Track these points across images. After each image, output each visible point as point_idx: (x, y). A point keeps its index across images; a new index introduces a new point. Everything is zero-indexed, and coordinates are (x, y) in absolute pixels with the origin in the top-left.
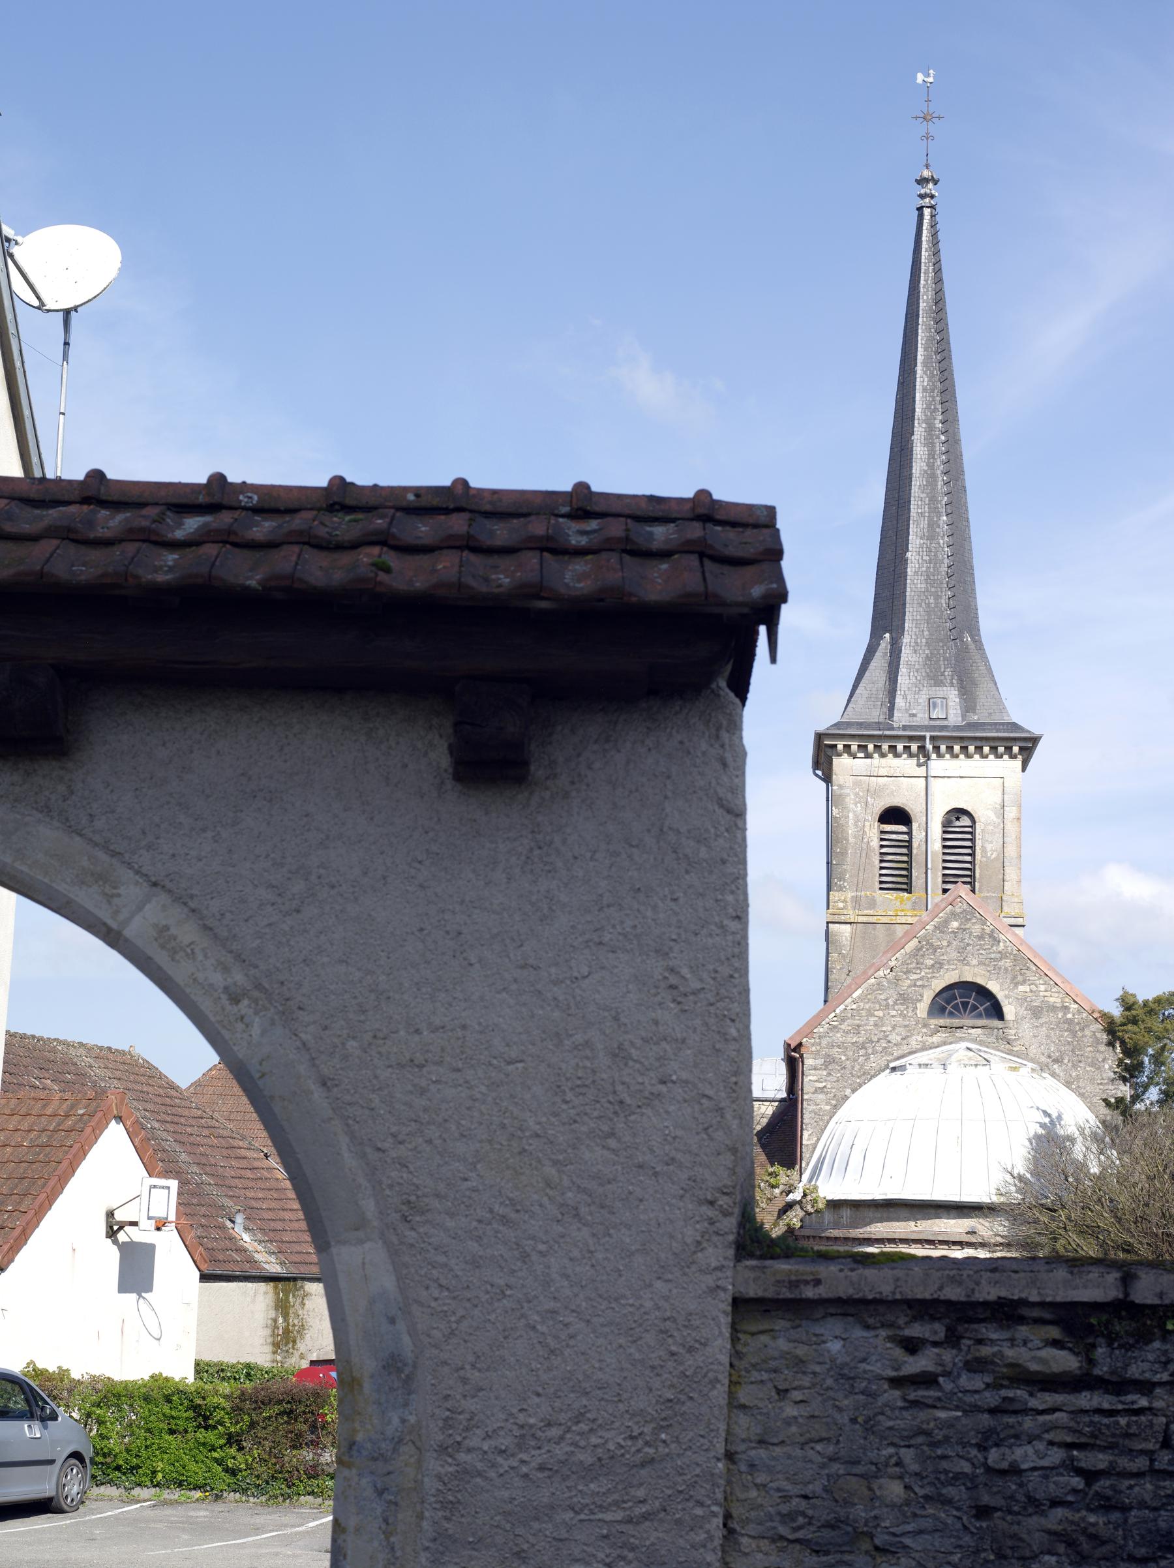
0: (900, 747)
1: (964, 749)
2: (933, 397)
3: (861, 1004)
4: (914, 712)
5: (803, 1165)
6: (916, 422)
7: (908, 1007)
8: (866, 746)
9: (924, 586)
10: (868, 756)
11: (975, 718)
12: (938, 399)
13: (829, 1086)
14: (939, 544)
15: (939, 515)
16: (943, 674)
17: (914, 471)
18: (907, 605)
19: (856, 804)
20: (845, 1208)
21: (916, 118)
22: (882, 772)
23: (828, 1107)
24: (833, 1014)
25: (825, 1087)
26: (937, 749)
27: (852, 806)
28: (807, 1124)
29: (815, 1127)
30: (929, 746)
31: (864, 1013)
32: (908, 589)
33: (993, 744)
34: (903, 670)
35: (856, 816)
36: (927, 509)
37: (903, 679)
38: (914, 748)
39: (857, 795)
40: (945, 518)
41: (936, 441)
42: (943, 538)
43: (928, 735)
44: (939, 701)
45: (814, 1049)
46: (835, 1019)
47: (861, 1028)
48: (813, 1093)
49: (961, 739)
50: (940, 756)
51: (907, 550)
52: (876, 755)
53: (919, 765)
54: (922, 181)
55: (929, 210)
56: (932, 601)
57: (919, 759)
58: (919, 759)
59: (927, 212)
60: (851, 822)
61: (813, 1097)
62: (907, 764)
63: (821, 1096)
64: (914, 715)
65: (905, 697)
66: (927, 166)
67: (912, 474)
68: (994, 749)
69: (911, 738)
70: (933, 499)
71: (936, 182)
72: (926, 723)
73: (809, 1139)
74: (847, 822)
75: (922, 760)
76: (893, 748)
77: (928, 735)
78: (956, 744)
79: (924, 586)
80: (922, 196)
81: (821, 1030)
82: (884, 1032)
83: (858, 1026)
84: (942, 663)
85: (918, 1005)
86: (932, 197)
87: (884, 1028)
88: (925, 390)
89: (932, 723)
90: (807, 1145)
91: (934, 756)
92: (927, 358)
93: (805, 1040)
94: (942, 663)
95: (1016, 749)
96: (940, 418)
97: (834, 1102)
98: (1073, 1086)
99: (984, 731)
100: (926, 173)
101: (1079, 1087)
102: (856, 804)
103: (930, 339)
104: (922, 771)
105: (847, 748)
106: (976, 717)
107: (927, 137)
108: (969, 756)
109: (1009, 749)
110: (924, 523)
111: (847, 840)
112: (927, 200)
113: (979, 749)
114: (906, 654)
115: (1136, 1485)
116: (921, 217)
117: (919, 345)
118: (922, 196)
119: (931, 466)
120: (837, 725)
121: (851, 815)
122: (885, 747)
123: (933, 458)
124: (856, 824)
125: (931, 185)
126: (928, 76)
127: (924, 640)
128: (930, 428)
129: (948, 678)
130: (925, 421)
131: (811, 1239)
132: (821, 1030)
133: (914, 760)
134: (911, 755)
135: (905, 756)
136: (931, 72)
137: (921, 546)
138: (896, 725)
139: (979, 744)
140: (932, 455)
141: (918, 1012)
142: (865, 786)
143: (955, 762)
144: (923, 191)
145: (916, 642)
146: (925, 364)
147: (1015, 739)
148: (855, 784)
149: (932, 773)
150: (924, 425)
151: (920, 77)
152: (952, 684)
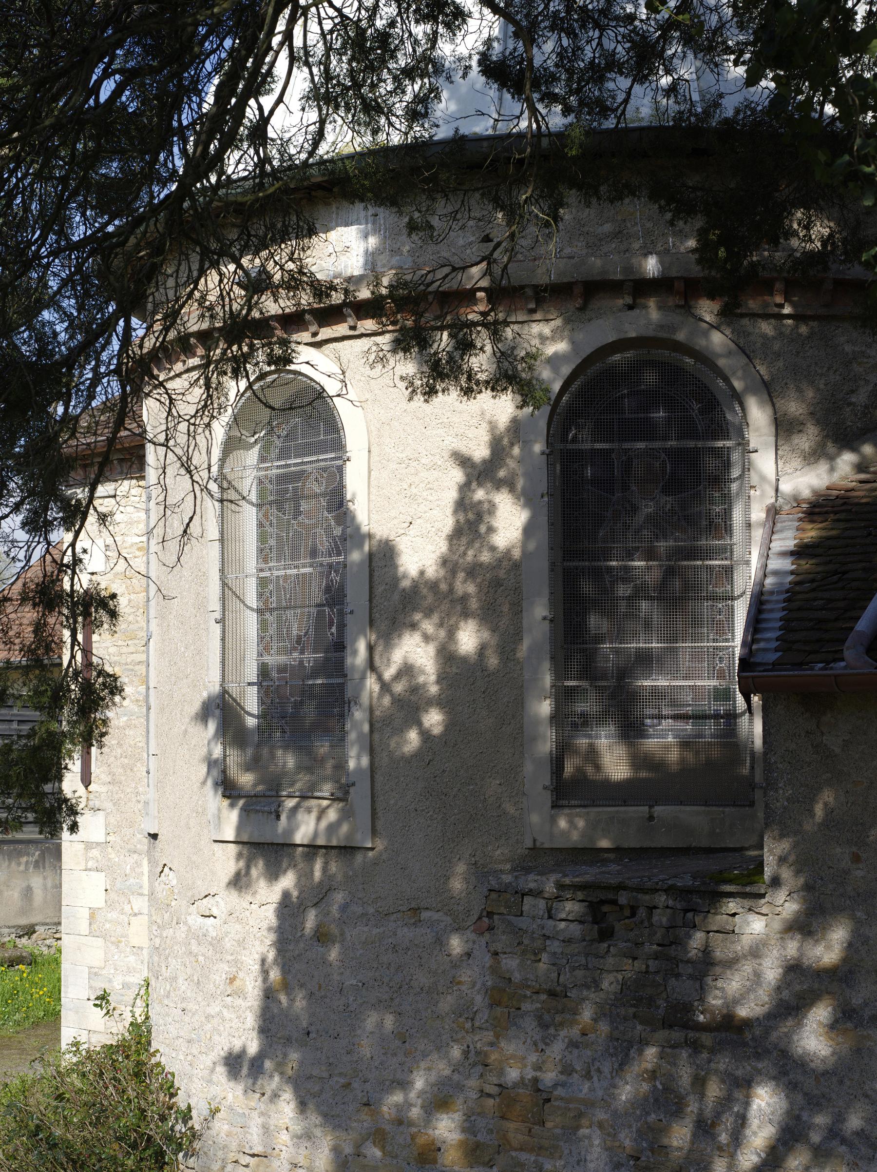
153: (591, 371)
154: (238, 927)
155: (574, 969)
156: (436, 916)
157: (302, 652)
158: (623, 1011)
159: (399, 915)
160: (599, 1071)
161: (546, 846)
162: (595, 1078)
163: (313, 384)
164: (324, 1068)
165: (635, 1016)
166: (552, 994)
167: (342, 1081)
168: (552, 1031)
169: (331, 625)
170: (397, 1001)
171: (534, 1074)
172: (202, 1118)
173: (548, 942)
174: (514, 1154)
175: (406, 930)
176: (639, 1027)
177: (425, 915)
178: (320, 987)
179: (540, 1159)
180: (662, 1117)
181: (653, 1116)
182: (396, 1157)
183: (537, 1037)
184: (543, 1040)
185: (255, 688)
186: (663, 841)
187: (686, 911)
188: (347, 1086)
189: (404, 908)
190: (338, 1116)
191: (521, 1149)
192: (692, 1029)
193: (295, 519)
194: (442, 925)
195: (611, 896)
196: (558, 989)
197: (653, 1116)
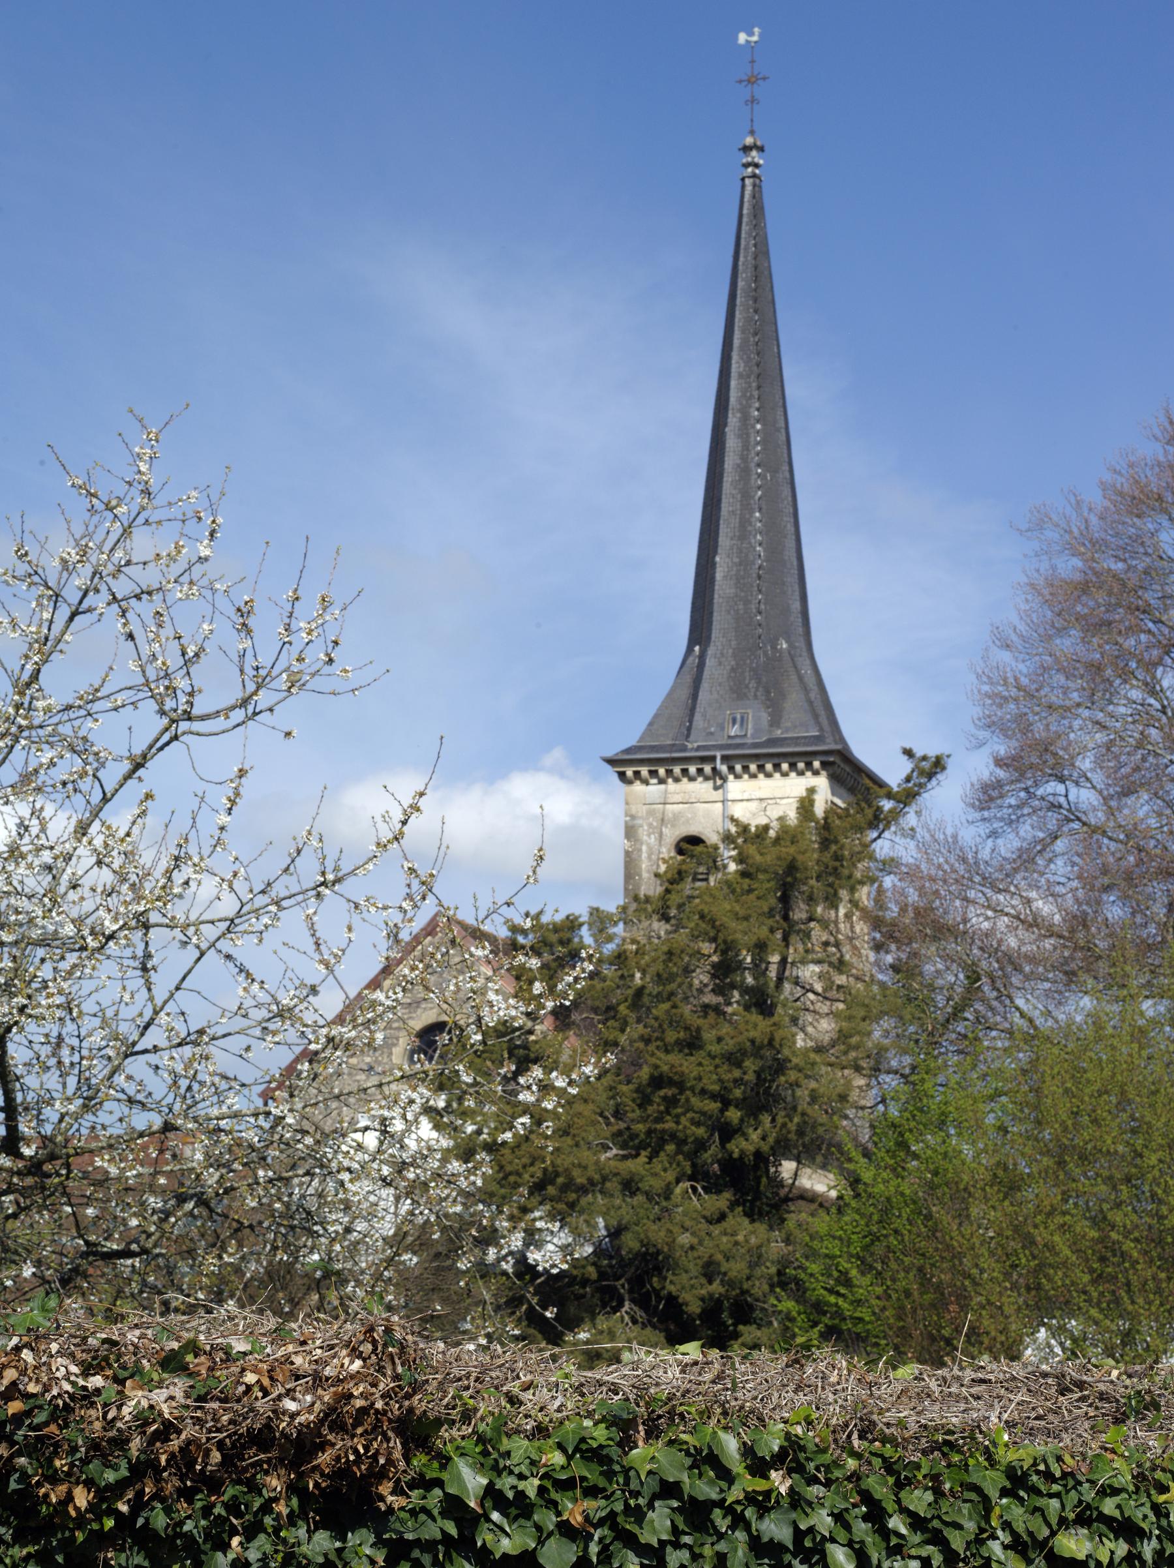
0: (692, 770)
1: (761, 768)
2: (749, 383)
4: (712, 729)
6: (730, 412)
8: (656, 771)
9: (733, 591)
10: (662, 781)
11: (778, 733)
12: (754, 385)
14: (750, 543)
15: (752, 512)
16: (747, 687)
17: (726, 466)
18: (715, 614)
19: (649, 835)
21: (740, 81)
22: (678, 798)
26: (731, 769)
27: (645, 838)
30: (724, 768)
32: (716, 596)
33: (792, 760)
34: (705, 685)
35: (650, 848)
36: (738, 507)
37: (703, 696)
38: (707, 769)
39: (650, 825)
40: (757, 514)
41: (751, 431)
42: (755, 537)
43: (718, 755)
44: (738, 717)
49: (756, 757)
50: (737, 777)
51: (715, 553)
52: (670, 780)
53: (716, 788)
54: (746, 149)
55: (752, 180)
56: (741, 607)
57: (715, 782)
58: (715, 782)
59: (748, 182)
60: (644, 855)
62: (702, 788)
64: (712, 734)
65: (704, 715)
66: (752, 133)
67: (723, 470)
68: (793, 766)
69: (704, 760)
70: (746, 495)
71: (761, 149)
72: (724, 742)
74: (640, 856)
75: (719, 782)
76: (685, 772)
77: (718, 755)
78: (752, 762)
79: (733, 591)
80: (746, 165)
84: (747, 674)
85: (394, 1050)
86: (757, 166)
88: (740, 376)
89: (730, 742)
91: (731, 777)
92: (744, 341)
94: (747, 674)
95: (816, 764)
96: (757, 405)
99: (781, 746)
100: (749, 141)
102: (649, 835)
103: (748, 320)
104: (718, 795)
105: (637, 774)
106: (779, 732)
107: (753, 101)
108: (768, 775)
109: (809, 765)
110: (735, 521)
111: (640, 875)
112: (750, 170)
113: (793, 766)
114: (710, 662)
115: (903, 1510)
116: (743, 187)
117: (736, 328)
118: (746, 165)
119: (744, 458)
120: (628, 751)
121: (644, 848)
122: (677, 770)
123: (748, 450)
124: (649, 858)
125: (754, 153)
126: (751, 34)
127: (731, 651)
128: (745, 418)
129: (753, 690)
130: (740, 411)
131: (243, 975)
133: (710, 784)
134: (707, 779)
135: (700, 779)
136: (756, 30)
137: (731, 548)
138: (690, 746)
139: (776, 761)
140: (746, 447)
141: (394, 1058)
142: (659, 816)
143: (753, 783)
144: (744, 161)
145: (722, 654)
146: (741, 348)
147: (814, 754)
148: (651, 813)
149: (730, 796)
150: (738, 415)
151: (742, 38)
152: (756, 697)
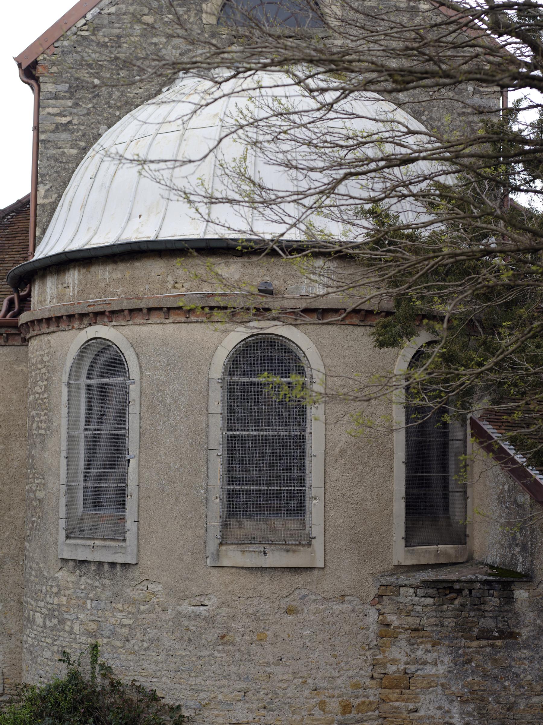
3: (123, 6)
5: (38, 234)
7: (189, 10)
13: (75, 121)
20: (71, 272)
23: (74, 152)
24: (83, 21)
25: (70, 122)
28: (42, 176)
29: (55, 180)
31: (127, 18)
45: (54, 69)
46: (86, 27)
47: (123, 40)
48: (53, 132)
61: (53, 137)
63: (65, 136)
73: (45, 197)
81: (66, 43)
82: (156, 44)
83: (119, 37)
87: (155, 40)
90: (43, 205)
93: (41, 58)
97: (82, 144)
98: (424, 118)
101: (431, 118)
132: (66, 43)
153: (90, 343)
154: (228, 610)
155: (429, 618)
156: (352, 598)
157: (260, 471)
158: (455, 634)
159: (335, 599)
160: (442, 662)
161: (403, 564)
162: (439, 665)
163: (259, 337)
164: (290, 675)
165: (462, 636)
166: (416, 630)
167: (301, 680)
168: (416, 646)
169: (281, 459)
170: (333, 640)
171: (405, 666)
172: (334, 705)
173: (415, 607)
174: (391, 704)
175: (338, 606)
176: (464, 641)
177: (347, 598)
178: (289, 636)
179: (407, 704)
180: (475, 677)
181: (471, 678)
182: (331, 713)
183: (408, 650)
184: (411, 650)
185: (450, 489)
186: (442, 561)
187: (489, 590)
188: (305, 682)
189: (339, 595)
190: (299, 697)
191: (397, 701)
192: (491, 639)
193: (255, 405)
194: (355, 602)
195: (450, 585)
196: (420, 627)
197: (471, 678)
